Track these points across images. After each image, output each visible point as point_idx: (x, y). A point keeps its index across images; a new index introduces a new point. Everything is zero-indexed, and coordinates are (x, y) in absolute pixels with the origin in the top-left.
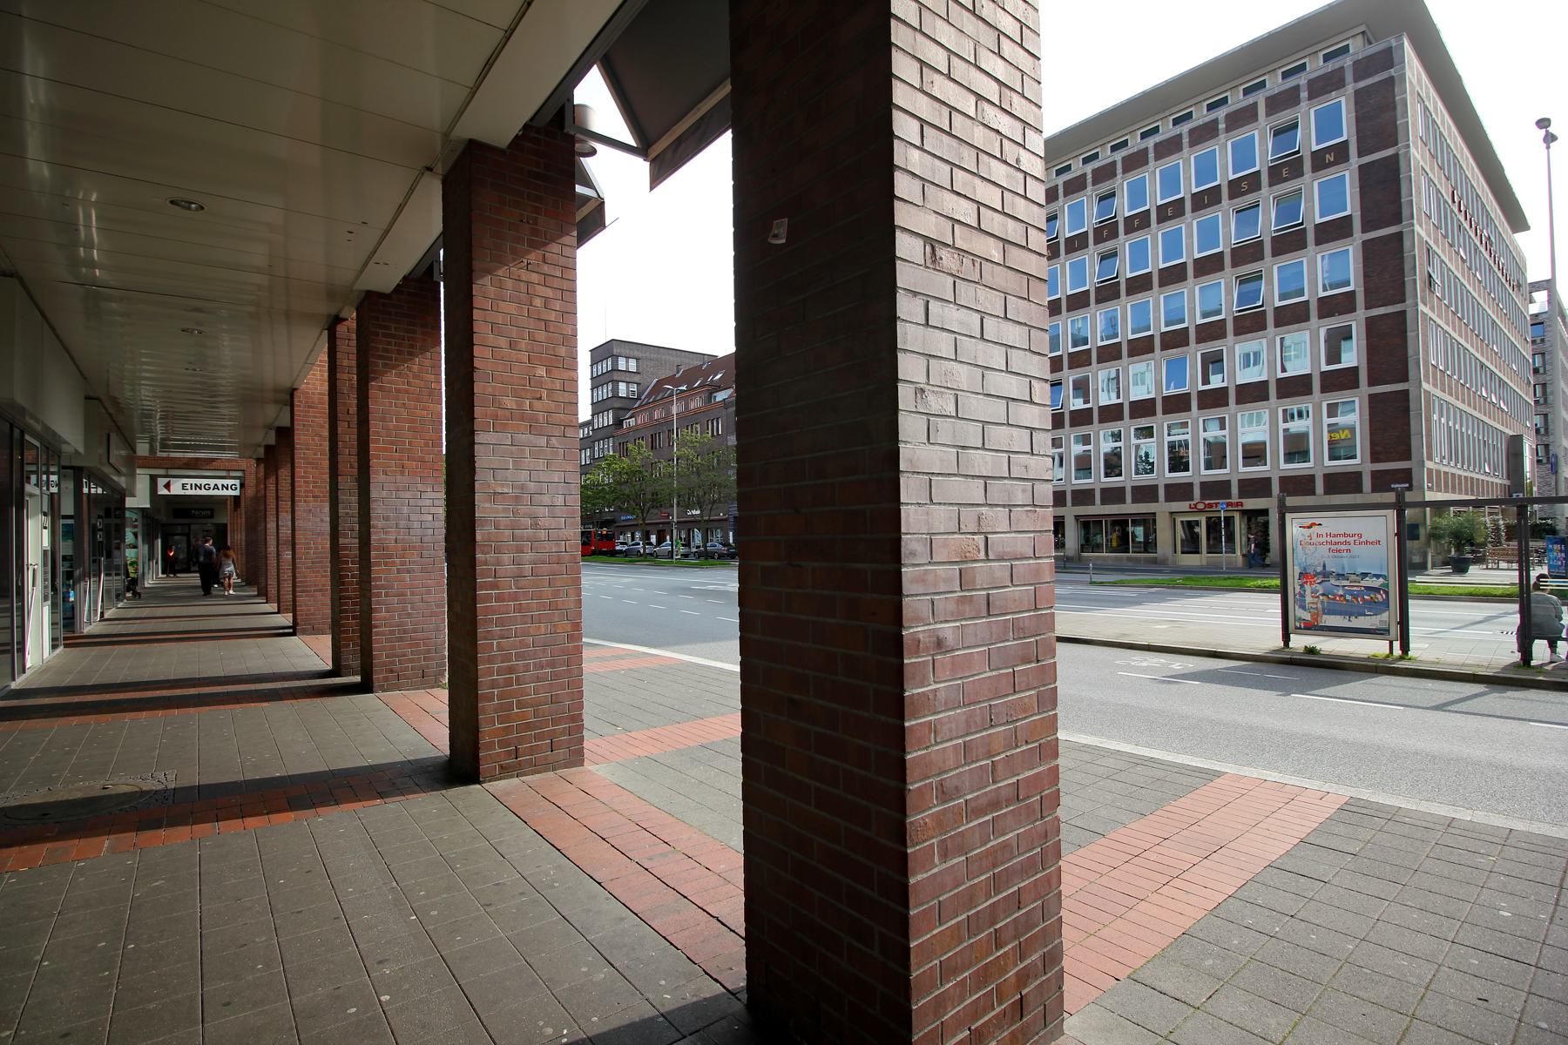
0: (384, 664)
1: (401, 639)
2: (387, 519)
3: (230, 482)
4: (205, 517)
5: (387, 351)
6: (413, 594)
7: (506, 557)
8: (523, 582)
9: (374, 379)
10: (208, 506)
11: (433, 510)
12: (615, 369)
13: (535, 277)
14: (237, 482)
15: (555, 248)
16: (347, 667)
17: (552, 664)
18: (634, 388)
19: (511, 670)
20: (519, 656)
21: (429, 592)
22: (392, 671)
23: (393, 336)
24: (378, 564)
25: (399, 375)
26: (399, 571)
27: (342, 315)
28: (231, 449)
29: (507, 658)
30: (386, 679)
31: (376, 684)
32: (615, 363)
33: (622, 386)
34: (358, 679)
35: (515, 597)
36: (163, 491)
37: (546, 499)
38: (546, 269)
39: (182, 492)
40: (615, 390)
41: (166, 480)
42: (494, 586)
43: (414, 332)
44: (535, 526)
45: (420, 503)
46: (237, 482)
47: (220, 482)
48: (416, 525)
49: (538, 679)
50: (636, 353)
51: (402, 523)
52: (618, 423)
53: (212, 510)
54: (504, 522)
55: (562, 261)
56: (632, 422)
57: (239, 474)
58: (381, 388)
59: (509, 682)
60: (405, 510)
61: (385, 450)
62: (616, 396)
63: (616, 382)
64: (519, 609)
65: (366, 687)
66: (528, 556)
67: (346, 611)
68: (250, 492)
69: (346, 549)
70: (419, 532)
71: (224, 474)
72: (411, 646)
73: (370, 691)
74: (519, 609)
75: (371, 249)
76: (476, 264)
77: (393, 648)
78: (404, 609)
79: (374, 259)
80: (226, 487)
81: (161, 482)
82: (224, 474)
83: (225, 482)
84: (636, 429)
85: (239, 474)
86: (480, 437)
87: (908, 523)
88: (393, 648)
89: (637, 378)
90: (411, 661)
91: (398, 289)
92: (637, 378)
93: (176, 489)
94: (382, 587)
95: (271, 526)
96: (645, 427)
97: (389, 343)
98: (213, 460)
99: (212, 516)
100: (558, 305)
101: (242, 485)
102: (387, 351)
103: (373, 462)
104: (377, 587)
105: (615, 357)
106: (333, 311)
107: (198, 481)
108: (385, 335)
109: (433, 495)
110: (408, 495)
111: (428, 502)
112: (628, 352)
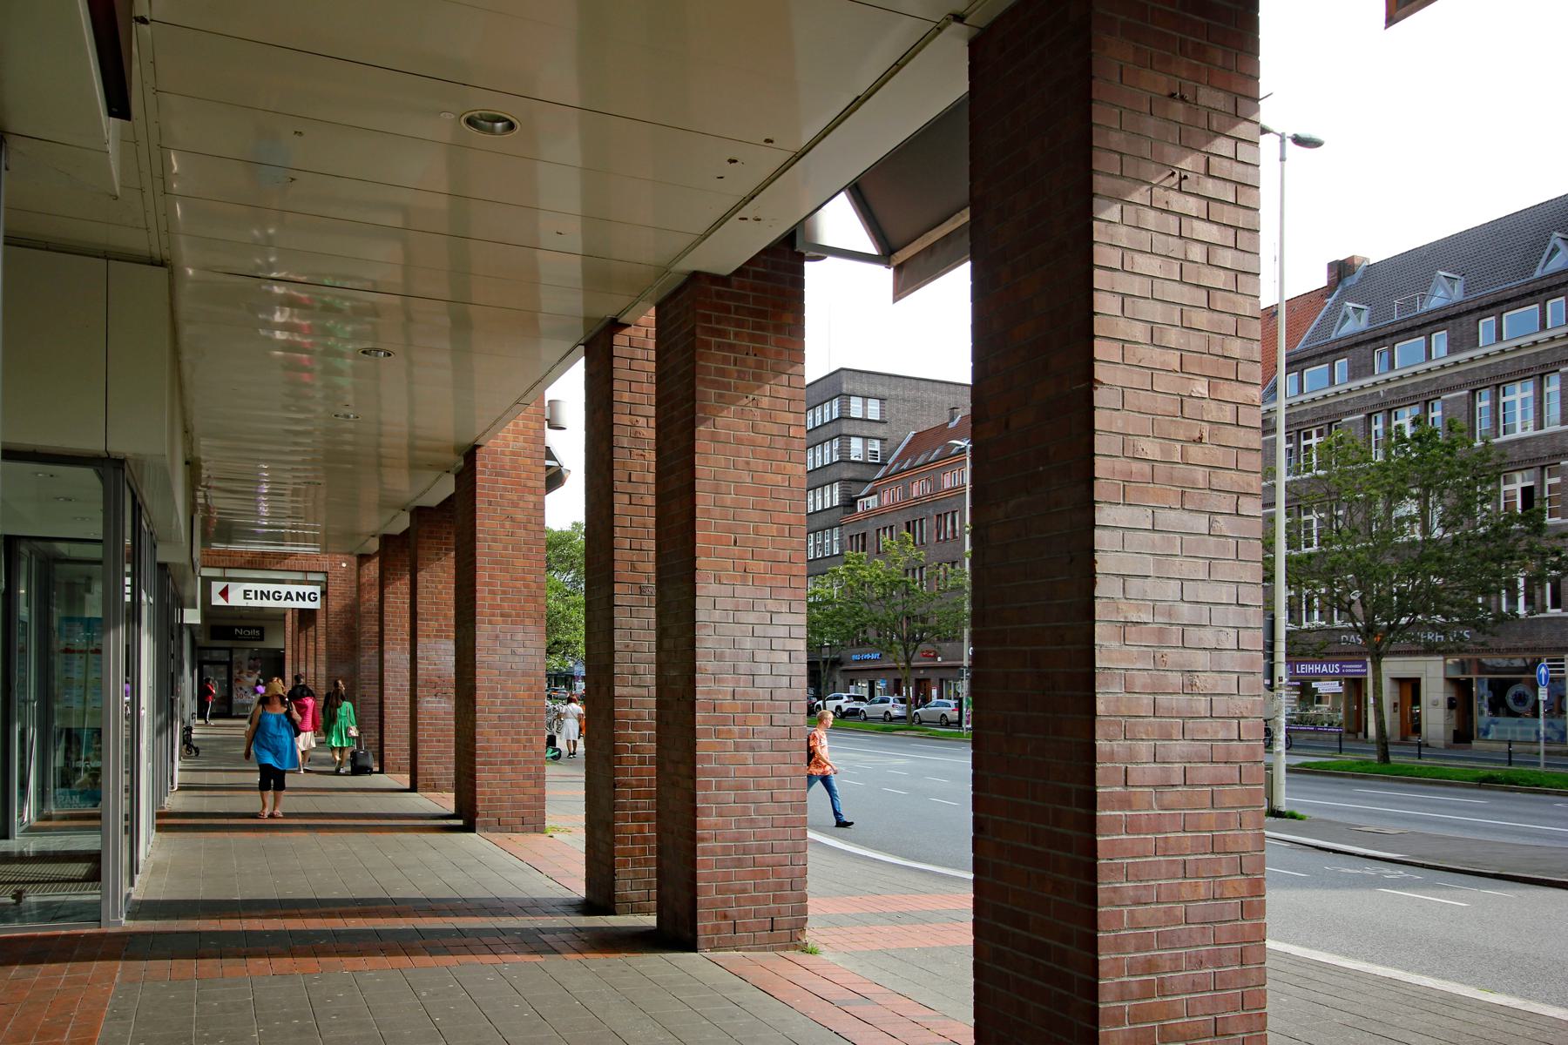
0: (713, 904)
1: (739, 863)
2: (719, 657)
3: (308, 589)
4: (250, 639)
5: (722, 373)
6: (758, 787)
7: (1144, 748)
8: (1170, 796)
9: (704, 420)
10: (257, 622)
11: (790, 644)
12: (844, 417)
13: (1192, 205)
14: (317, 589)
15: (1223, 146)
16: (626, 900)
17: (1217, 960)
18: (876, 446)
19: (1150, 966)
20: (1165, 940)
21: (781, 786)
22: (725, 917)
23: (731, 348)
24: (707, 734)
25: (741, 415)
26: (737, 747)
27: (624, 319)
28: (305, 538)
29: (1143, 944)
30: (717, 929)
31: (701, 937)
32: (844, 407)
33: (856, 445)
34: (651, 921)
35: (1156, 826)
36: (218, 601)
37: (1208, 637)
38: (1210, 188)
39: (243, 603)
40: (844, 450)
41: (222, 585)
42: (1126, 803)
43: (763, 340)
44: (1189, 689)
45: (771, 631)
46: (317, 589)
47: (294, 589)
48: (765, 669)
49: (1195, 987)
50: (881, 391)
51: (743, 667)
52: (849, 503)
53: (261, 629)
54: (1141, 680)
55: (1237, 172)
56: (872, 502)
57: (320, 577)
58: (714, 438)
59: (1147, 990)
60: (748, 643)
61: (719, 541)
62: (845, 460)
63: (845, 438)
64: (1162, 848)
65: (676, 933)
66: (1179, 747)
67: (623, 807)
68: (335, 605)
69: (623, 704)
70: (768, 681)
71: (299, 576)
72: (754, 875)
73: (690, 946)
74: (1162, 848)
75: (746, 192)
76: (1100, 183)
77: (727, 877)
78: (745, 812)
79: (747, 211)
80: (290, 594)
81: (217, 587)
82: (299, 576)
83: (302, 589)
84: (879, 513)
85: (320, 577)
86: (1103, 515)
87: (403, 649)
88: (727, 877)
89: (881, 431)
90: (755, 900)
91: (740, 272)
92: (881, 431)
93: (236, 599)
94: (713, 773)
95: (396, 657)
96: (896, 509)
97: (725, 360)
98: (286, 556)
99: (261, 638)
100: (1227, 258)
101: (324, 593)
102: (722, 373)
103: (701, 561)
104: (706, 773)
105: (845, 397)
106: (607, 311)
107: (265, 587)
108: (719, 347)
109: (790, 619)
110: (751, 617)
111: (783, 631)
112: (866, 389)
